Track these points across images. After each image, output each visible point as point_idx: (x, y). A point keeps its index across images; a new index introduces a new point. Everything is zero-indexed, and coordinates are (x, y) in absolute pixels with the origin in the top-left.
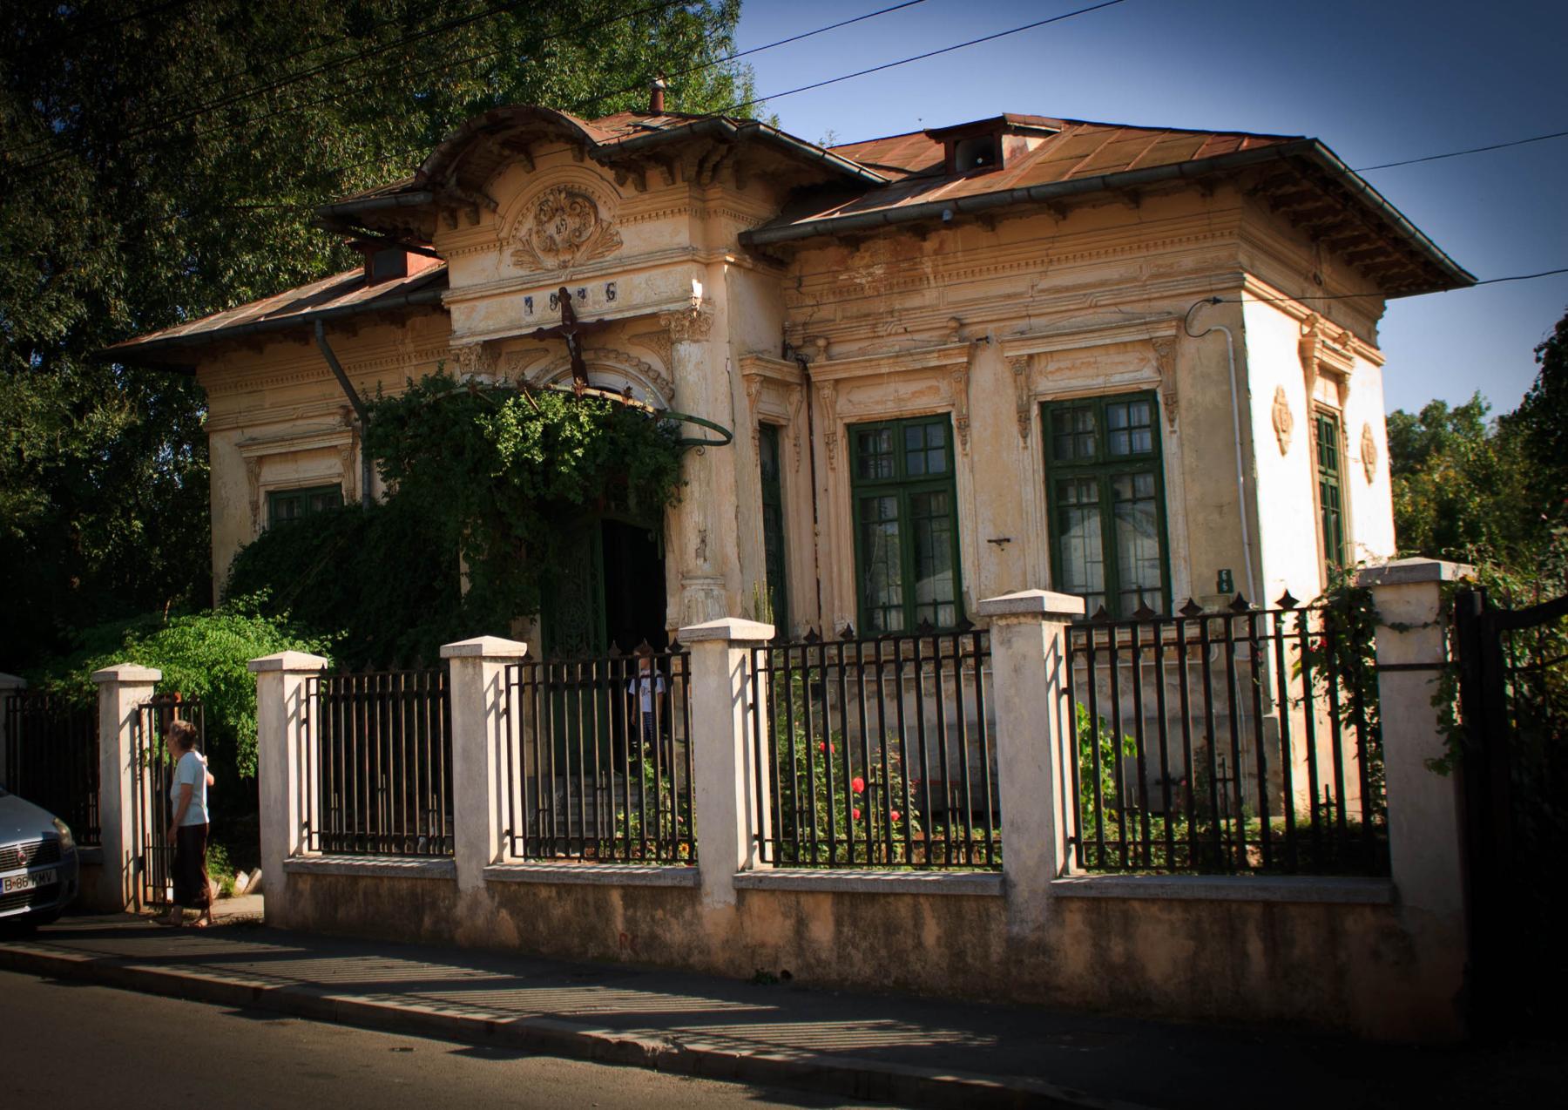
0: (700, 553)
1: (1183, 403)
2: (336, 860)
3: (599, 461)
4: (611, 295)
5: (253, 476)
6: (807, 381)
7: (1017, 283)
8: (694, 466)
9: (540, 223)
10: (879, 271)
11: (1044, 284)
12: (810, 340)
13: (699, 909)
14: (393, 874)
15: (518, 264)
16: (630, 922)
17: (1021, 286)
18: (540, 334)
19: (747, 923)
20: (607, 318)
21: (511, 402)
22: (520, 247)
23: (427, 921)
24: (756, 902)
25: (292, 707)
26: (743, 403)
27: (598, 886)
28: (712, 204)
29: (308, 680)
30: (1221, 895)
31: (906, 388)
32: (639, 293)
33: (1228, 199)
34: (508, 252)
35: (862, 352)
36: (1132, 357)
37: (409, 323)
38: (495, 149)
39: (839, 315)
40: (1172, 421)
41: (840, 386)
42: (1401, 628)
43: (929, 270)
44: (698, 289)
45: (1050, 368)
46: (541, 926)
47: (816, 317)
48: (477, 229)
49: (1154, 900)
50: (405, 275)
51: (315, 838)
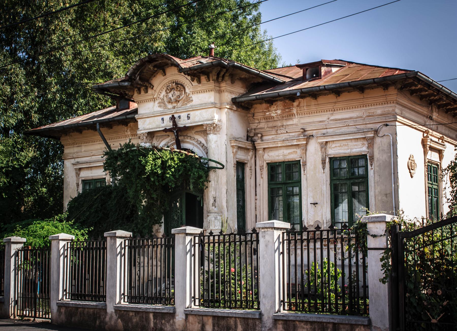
0: (214, 205)
1: (375, 159)
2: (73, 302)
3: (180, 173)
4: (188, 118)
5: (78, 175)
6: (255, 149)
7: (324, 117)
8: (212, 175)
9: (167, 93)
10: (279, 112)
11: (332, 118)
12: (256, 134)
13: (175, 320)
14: (88, 307)
15: (160, 106)
16: (155, 324)
17: (324, 118)
18: (165, 130)
19: (188, 325)
20: (187, 125)
21: (151, 153)
22: (160, 101)
23: (98, 322)
24: (191, 318)
25: (62, 251)
26: (231, 155)
27: (146, 313)
28: (222, 88)
29: (68, 243)
30: (320, 320)
31: (286, 151)
32: (198, 117)
33: (392, 91)
34: (157, 102)
35: (273, 139)
36: (360, 143)
37: (129, 125)
38: (152, 68)
39: (266, 126)
40: (371, 165)
41: (265, 150)
42: (374, 236)
43: (295, 112)
44: (216, 117)
45: (333, 146)
46: (130, 325)
47: (258, 127)
48: (147, 94)
49: (302, 321)
50: (129, 108)
51: (126, 297)
